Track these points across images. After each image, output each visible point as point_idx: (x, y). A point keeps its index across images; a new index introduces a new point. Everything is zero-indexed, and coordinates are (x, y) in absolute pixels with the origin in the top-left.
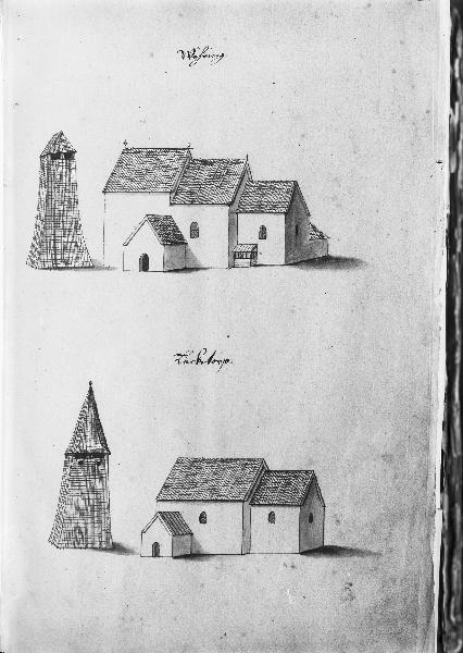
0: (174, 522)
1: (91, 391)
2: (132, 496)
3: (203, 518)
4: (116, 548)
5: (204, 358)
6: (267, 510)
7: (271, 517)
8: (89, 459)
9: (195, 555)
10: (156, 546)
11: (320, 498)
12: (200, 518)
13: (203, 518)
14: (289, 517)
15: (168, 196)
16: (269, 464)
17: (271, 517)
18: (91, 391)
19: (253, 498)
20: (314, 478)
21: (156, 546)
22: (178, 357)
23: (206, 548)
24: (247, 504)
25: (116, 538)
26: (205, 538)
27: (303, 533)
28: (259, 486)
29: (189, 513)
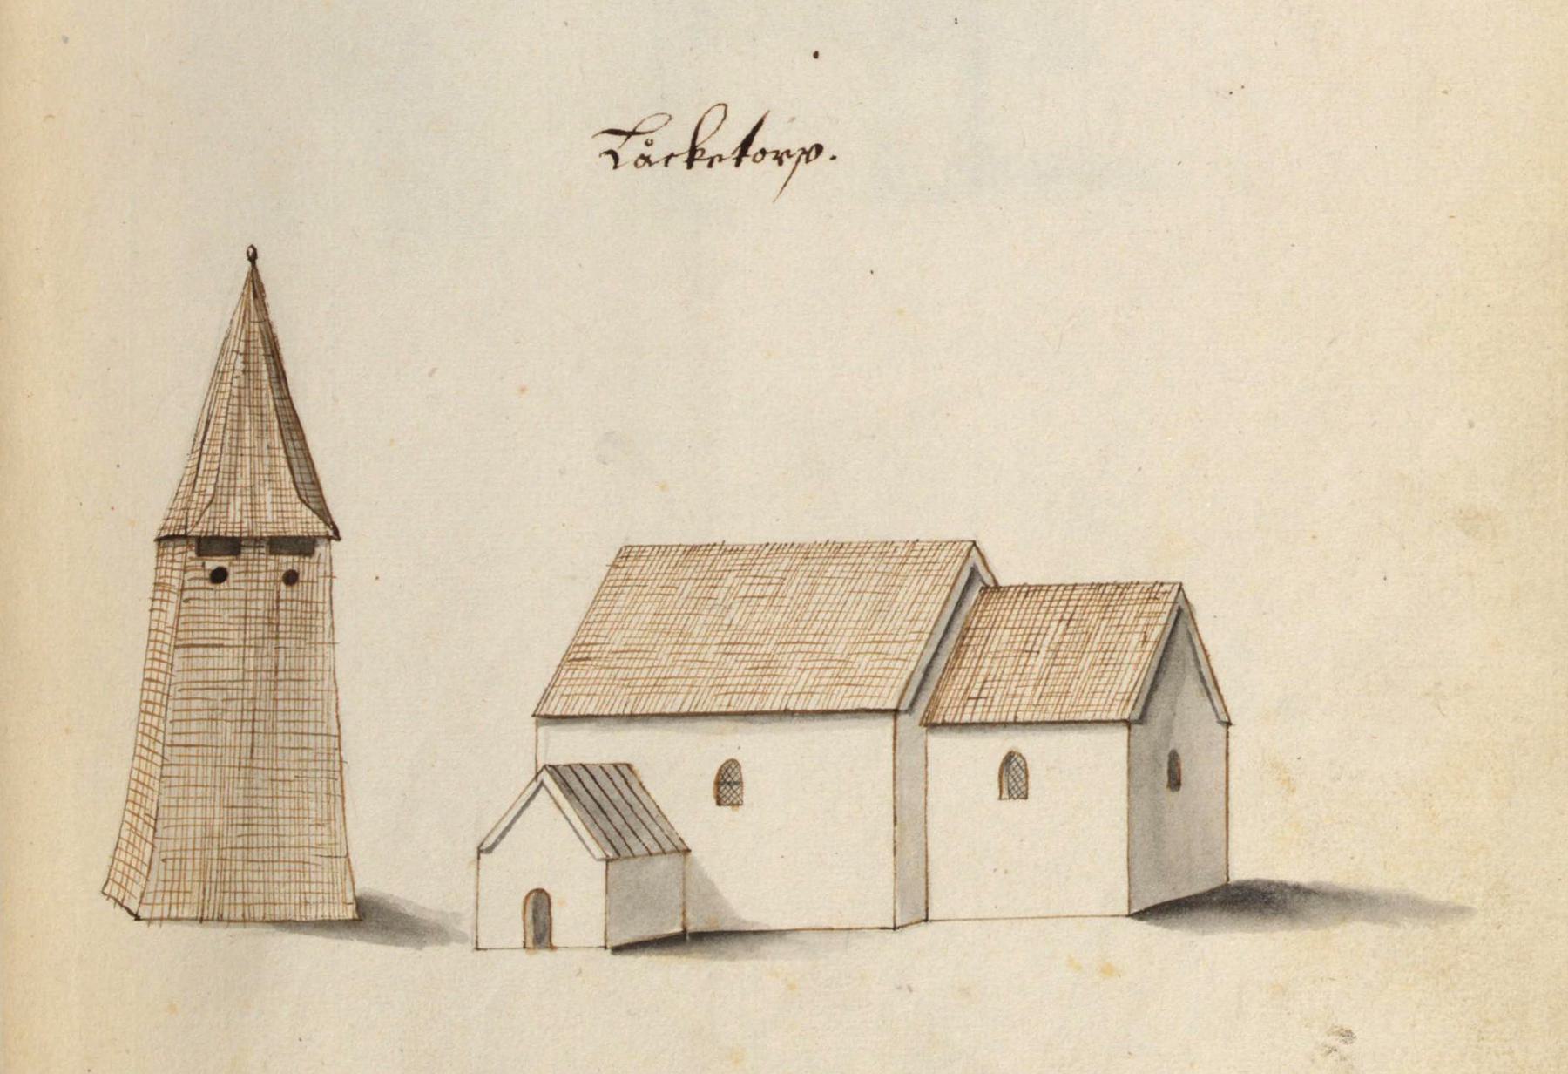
0: (610, 807)
1: (255, 287)
2: (429, 707)
3: (727, 785)
4: (371, 917)
5: (728, 142)
6: (995, 746)
7: (1013, 776)
8: (248, 549)
9: (480, 851)
10: (539, 905)
11: (1210, 687)
12: (719, 783)
13: (727, 785)
14: (1087, 774)
15: (1121, 734)
16: (994, 564)
17: (1013, 776)
18: (255, 287)
19: (924, 707)
20: (1182, 614)
21: (539, 905)
22: (614, 142)
23: (745, 905)
24: (908, 723)
25: (370, 882)
26: (739, 864)
27: (1146, 839)
28: (954, 636)
29: (674, 769)
